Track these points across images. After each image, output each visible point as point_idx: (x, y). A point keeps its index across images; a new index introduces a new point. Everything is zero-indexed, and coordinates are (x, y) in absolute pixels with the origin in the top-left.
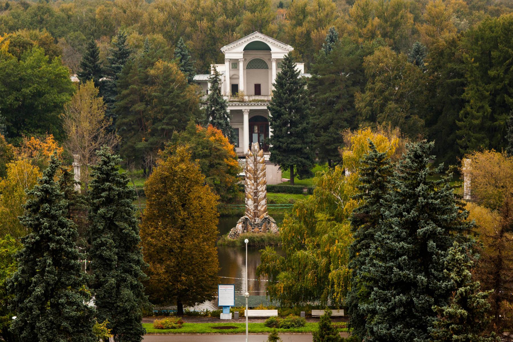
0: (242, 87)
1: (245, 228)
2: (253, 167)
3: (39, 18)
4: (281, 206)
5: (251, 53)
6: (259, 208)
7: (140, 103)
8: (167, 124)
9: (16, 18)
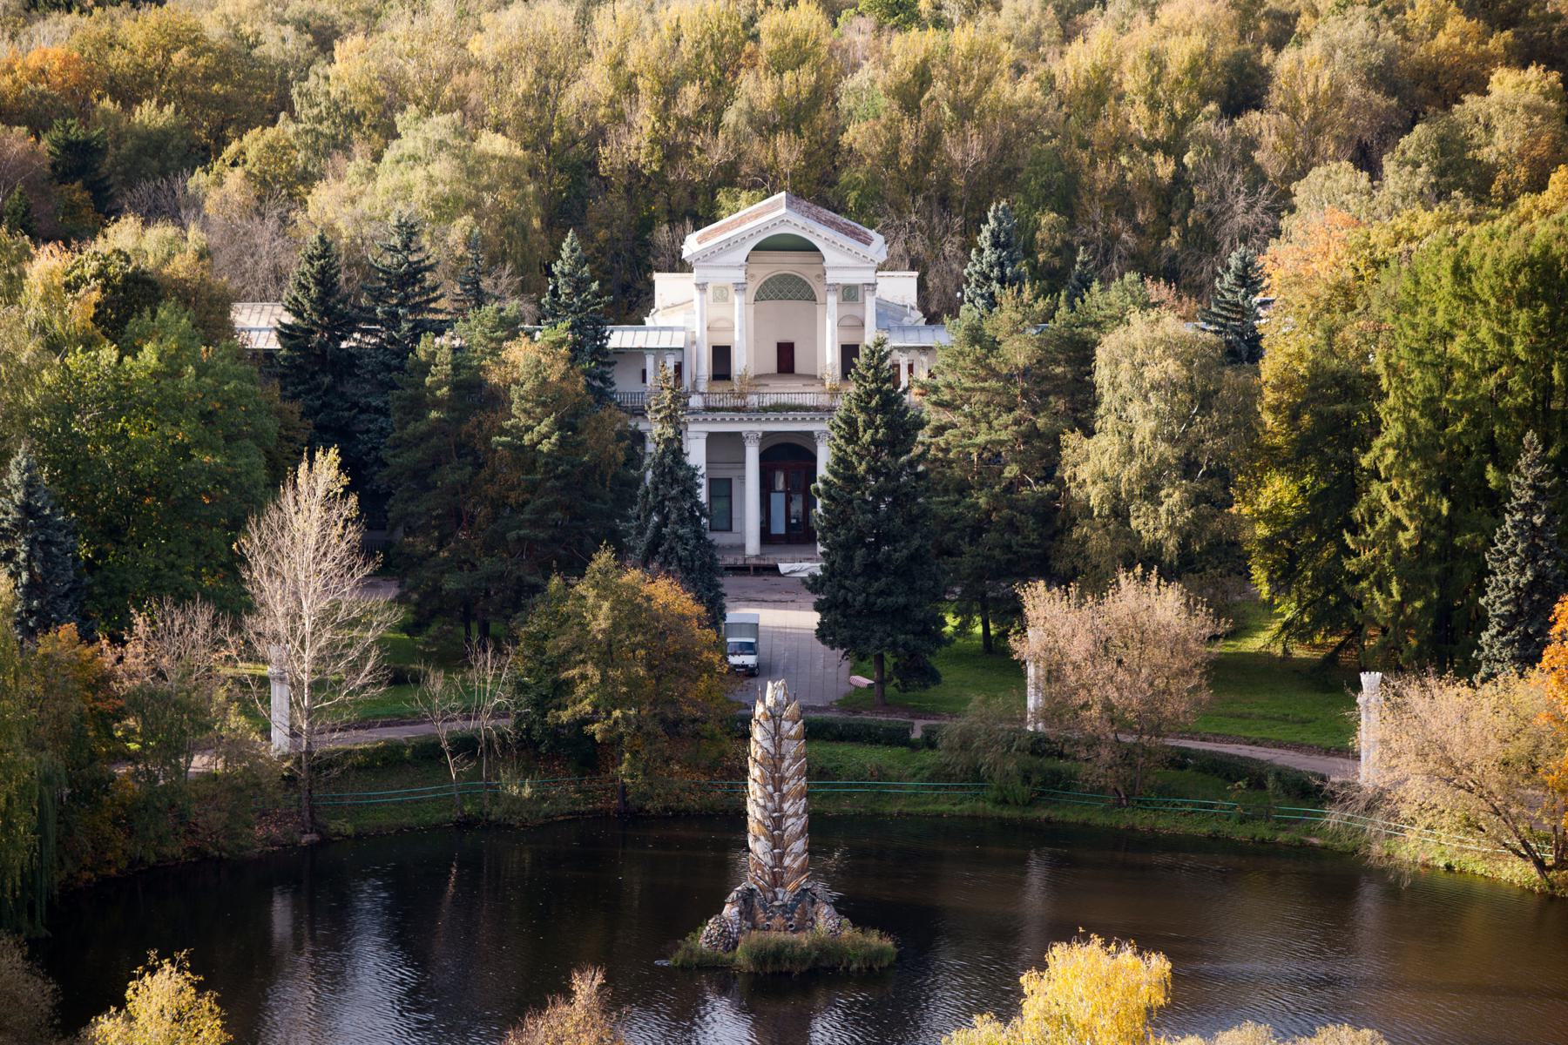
1: (747, 911)
4: (848, 786)
6: (787, 861)
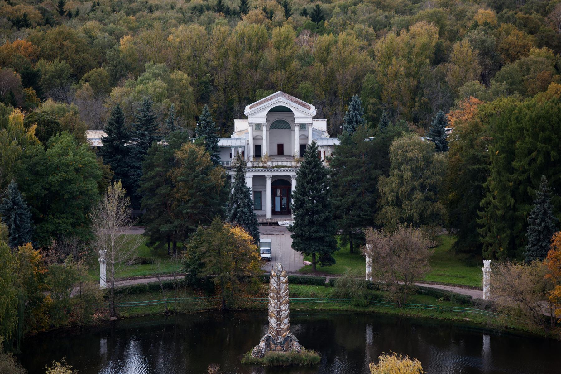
0: (265, 151)
1: (268, 345)
2: (277, 287)
3: (59, 44)
4: (304, 300)
5: (274, 115)
6: (282, 326)
7: (165, 186)
8: (192, 208)
9: (35, 44)
